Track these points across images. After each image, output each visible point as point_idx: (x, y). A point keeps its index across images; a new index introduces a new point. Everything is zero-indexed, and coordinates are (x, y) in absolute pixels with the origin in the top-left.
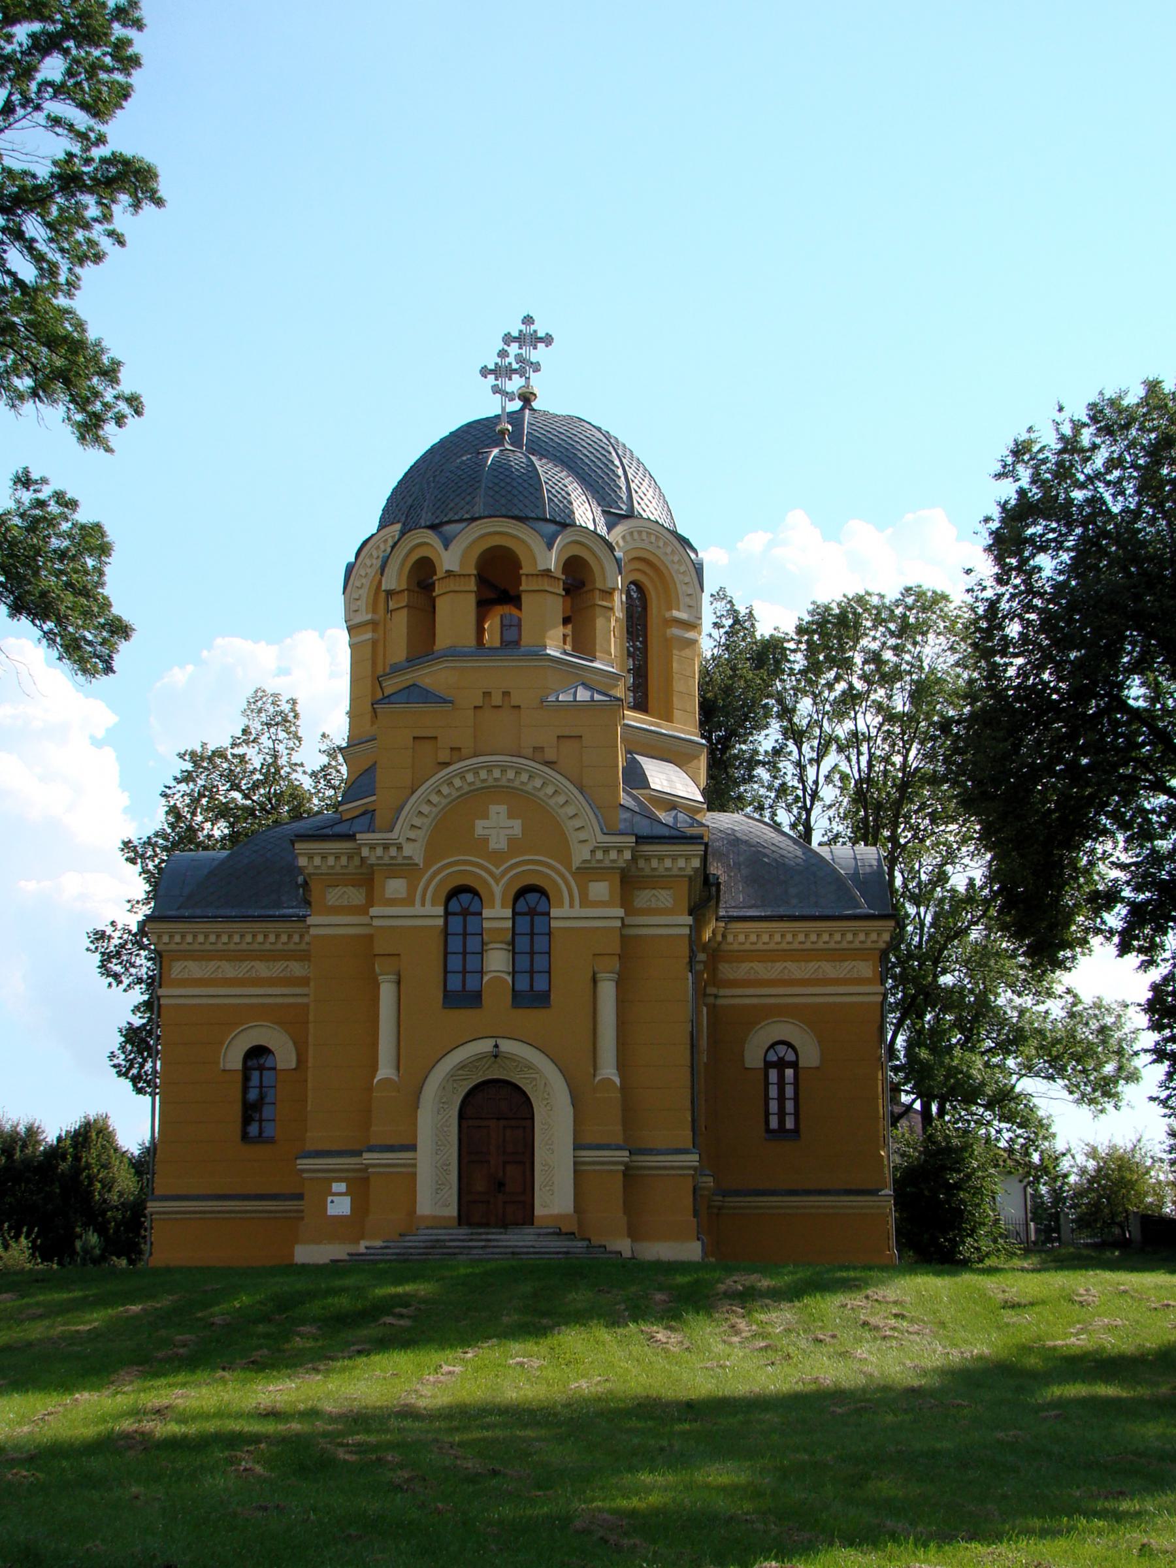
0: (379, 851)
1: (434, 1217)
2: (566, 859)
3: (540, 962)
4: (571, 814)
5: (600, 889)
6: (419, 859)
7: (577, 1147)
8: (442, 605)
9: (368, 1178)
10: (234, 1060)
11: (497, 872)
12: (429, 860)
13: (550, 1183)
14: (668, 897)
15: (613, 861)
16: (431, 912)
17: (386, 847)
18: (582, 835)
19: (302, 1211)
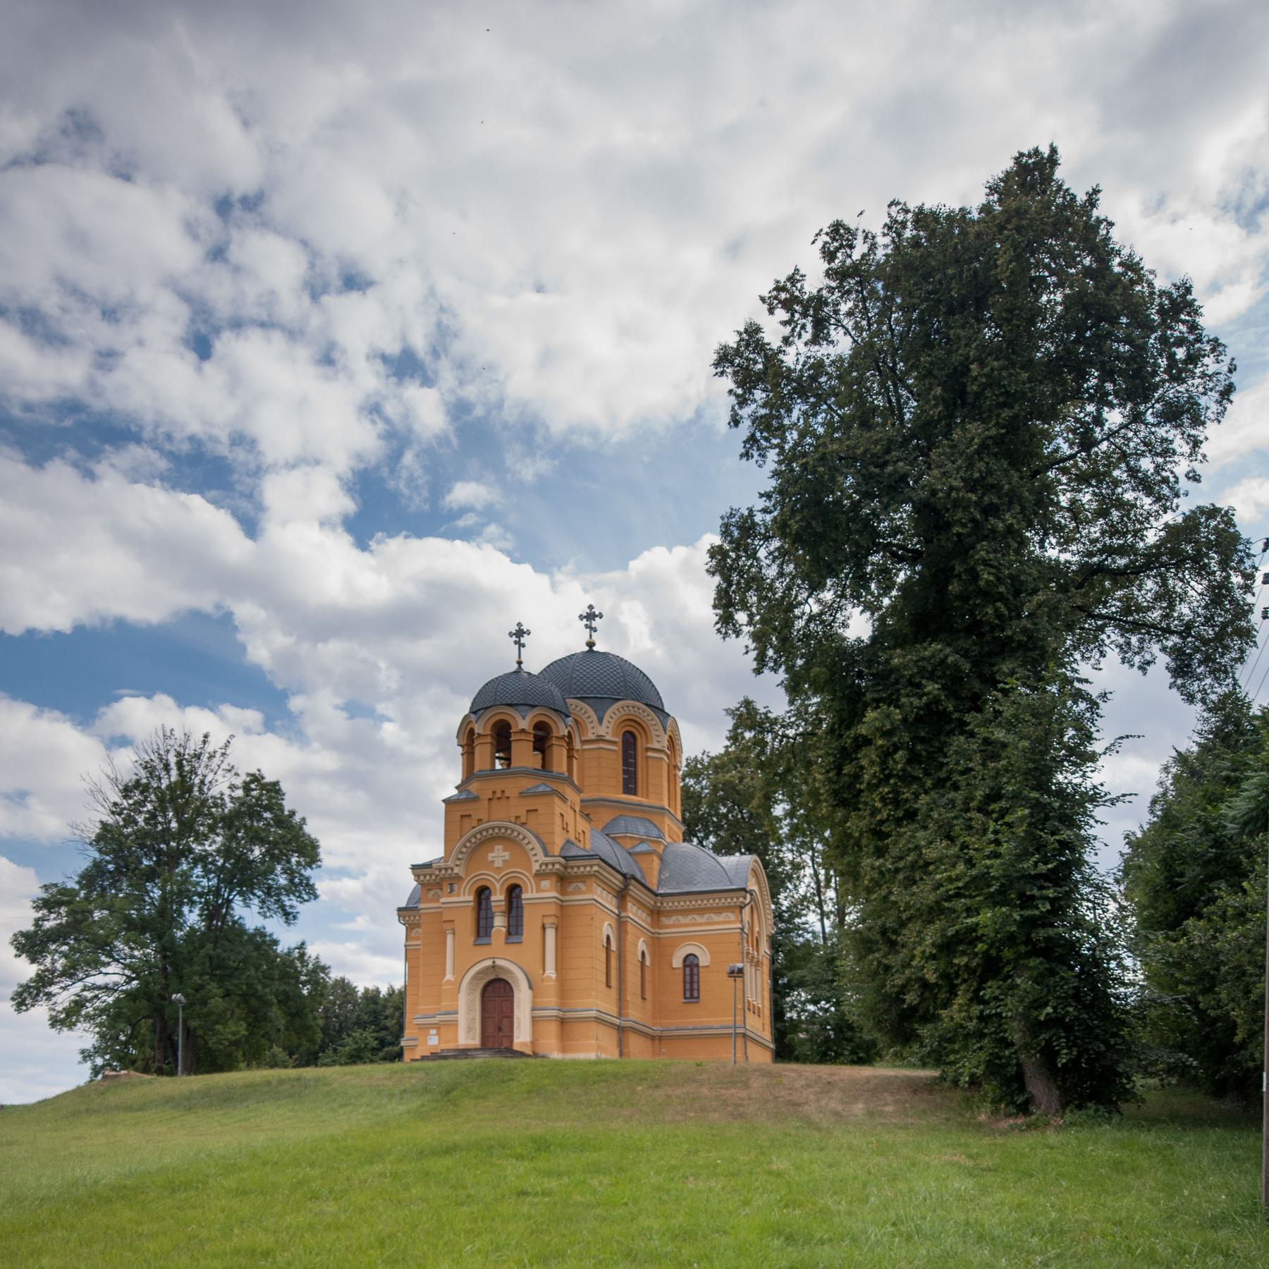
0: (443, 872)
2: (530, 870)
5: (545, 884)
6: (462, 874)
7: (533, 1009)
8: (477, 750)
10: (677, 962)
16: (468, 897)
18: (536, 858)
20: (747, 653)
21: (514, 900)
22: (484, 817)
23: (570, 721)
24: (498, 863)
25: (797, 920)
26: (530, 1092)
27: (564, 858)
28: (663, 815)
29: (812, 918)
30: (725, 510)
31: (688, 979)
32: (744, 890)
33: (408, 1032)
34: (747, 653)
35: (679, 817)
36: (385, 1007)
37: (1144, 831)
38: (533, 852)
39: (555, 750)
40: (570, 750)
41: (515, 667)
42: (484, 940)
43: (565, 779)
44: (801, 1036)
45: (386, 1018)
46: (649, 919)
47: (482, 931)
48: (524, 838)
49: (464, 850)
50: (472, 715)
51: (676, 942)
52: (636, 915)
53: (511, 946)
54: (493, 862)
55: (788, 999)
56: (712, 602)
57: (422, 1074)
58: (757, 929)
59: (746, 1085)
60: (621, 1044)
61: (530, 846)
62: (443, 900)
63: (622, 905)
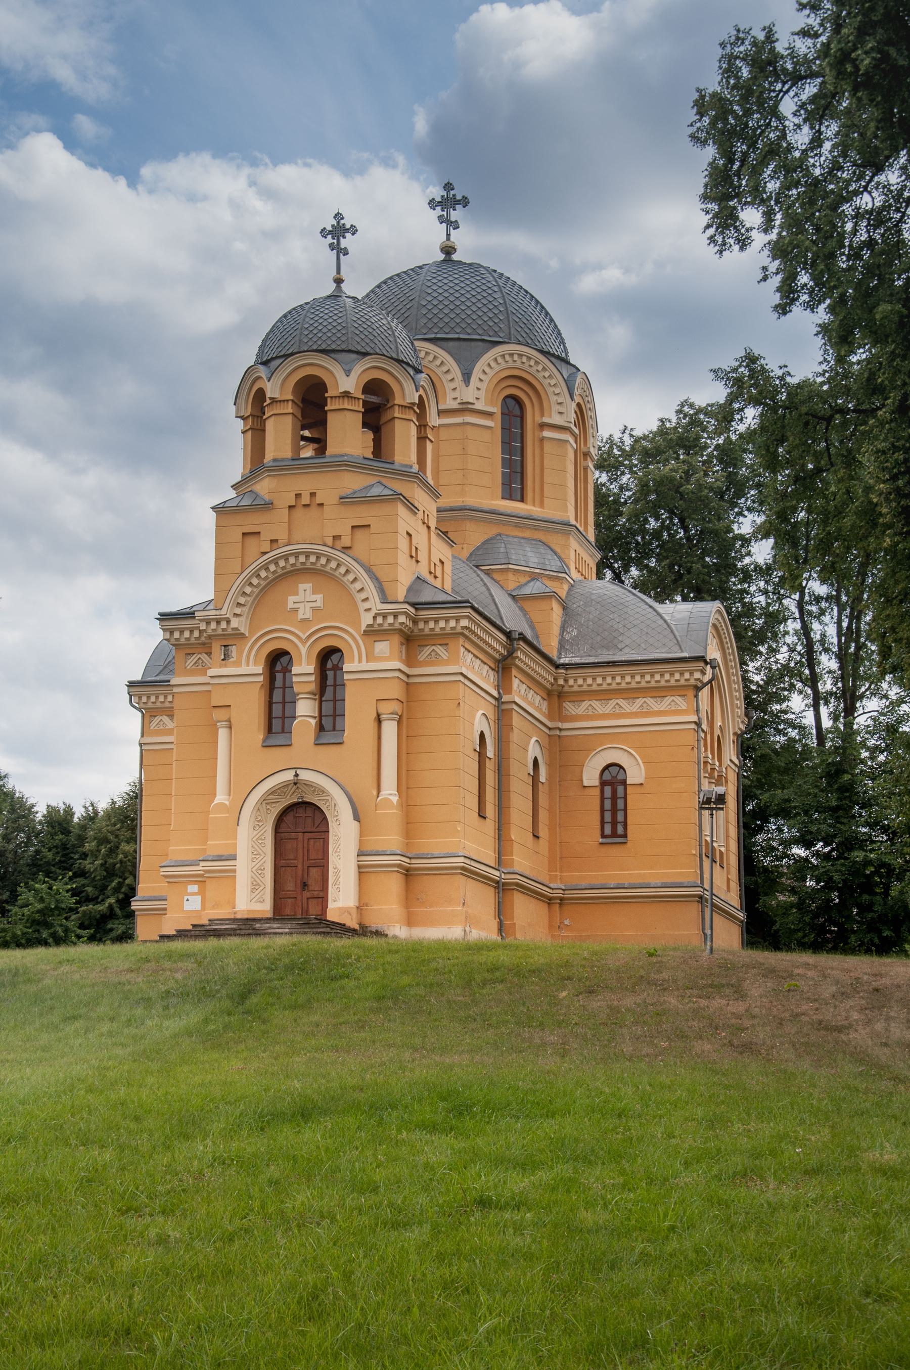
0: (213, 625)
2: (356, 623)
4: (358, 589)
5: (382, 647)
8: (270, 425)
10: (591, 776)
11: (304, 637)
12: (252, 630)
17: (218, 622)
18: (367, 605)
19: (165, 909)
20: (765, 279)
21: (330, 674)
22: (282, 536)
23: (422, 378)
24: (305, 612)
25: (776, 707)
26: (379, 998)
27: (413, 605)
28: (567, 534)
29: (797, 703)
30: (727, 32)
31: (608, 804)
32: (702, 659)
33: (145, 887)
34: (765, 279)
35: (591, 535)
36: (82, 839)
38: (363, 596)
39: (399, 426)
40: (422, 426)
41: (330, 288)
42: (280, 739)
43: (414, 476)
44: (781, 898)
45: (84, 856)
46: (545, 706)
47: (277, 724)
48: (347, 572)
49: (248, 590)
50: (261, 367)
51: (588, 745)
52: (525, 699)
53: (320, 747)
54: (295, 610)
55: (760, 837)
56: (702, 191)
57: (189, 965)
58: (718, 723)
59: (740, 994)
60: (501, 911)
61: (358, 586)
62: (212, 672)
63: (503, 684)
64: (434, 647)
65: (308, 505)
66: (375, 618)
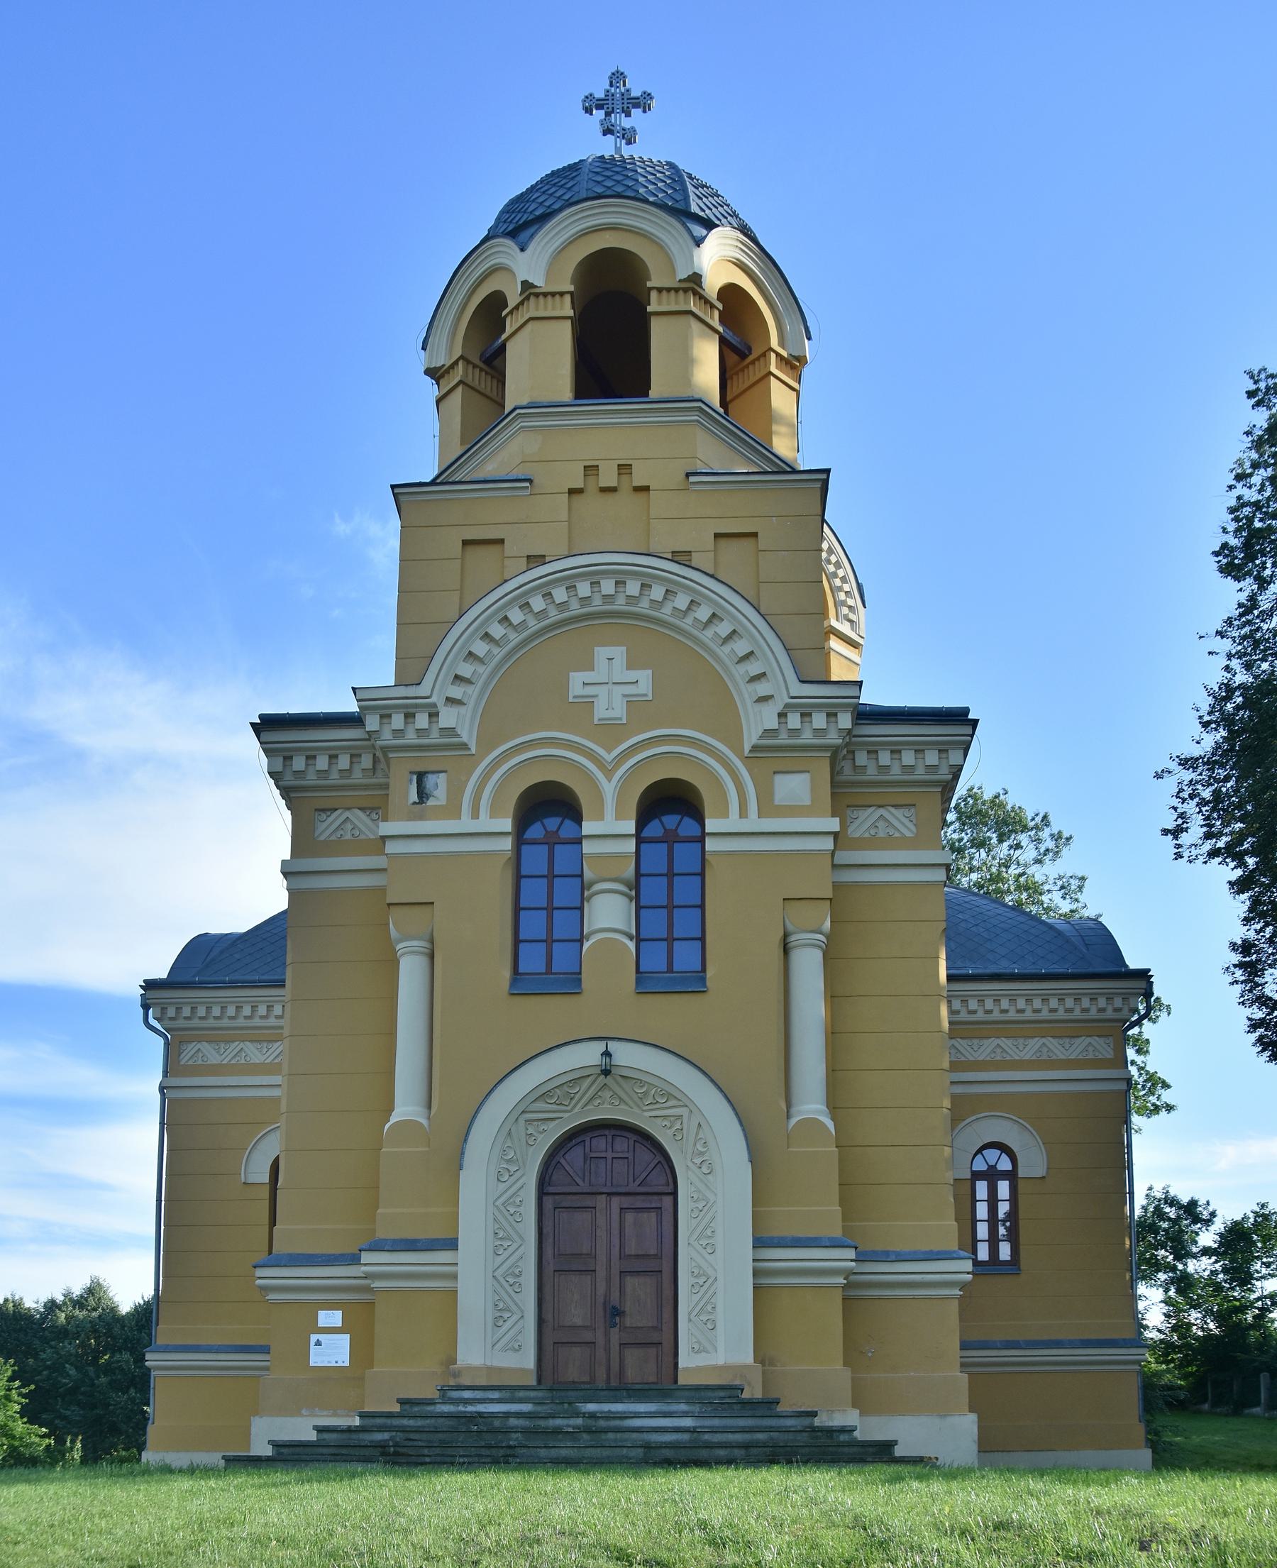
0: (398, 721)
1: (490, 1370)
2: (732, 735)
3: (685, 923)
6: (467, 735)
7: (759, 1243)
9: (372, 1304)
11: (609, 757)
12: (488, 739)
13: (709, 1308)
14: (906, 821)
15: (819, 732)
18: (762, 688)
24: (610, 706)
37: (144, 1301)
64: (882, 811)
65: (613, 490)
66: (782, 715)
